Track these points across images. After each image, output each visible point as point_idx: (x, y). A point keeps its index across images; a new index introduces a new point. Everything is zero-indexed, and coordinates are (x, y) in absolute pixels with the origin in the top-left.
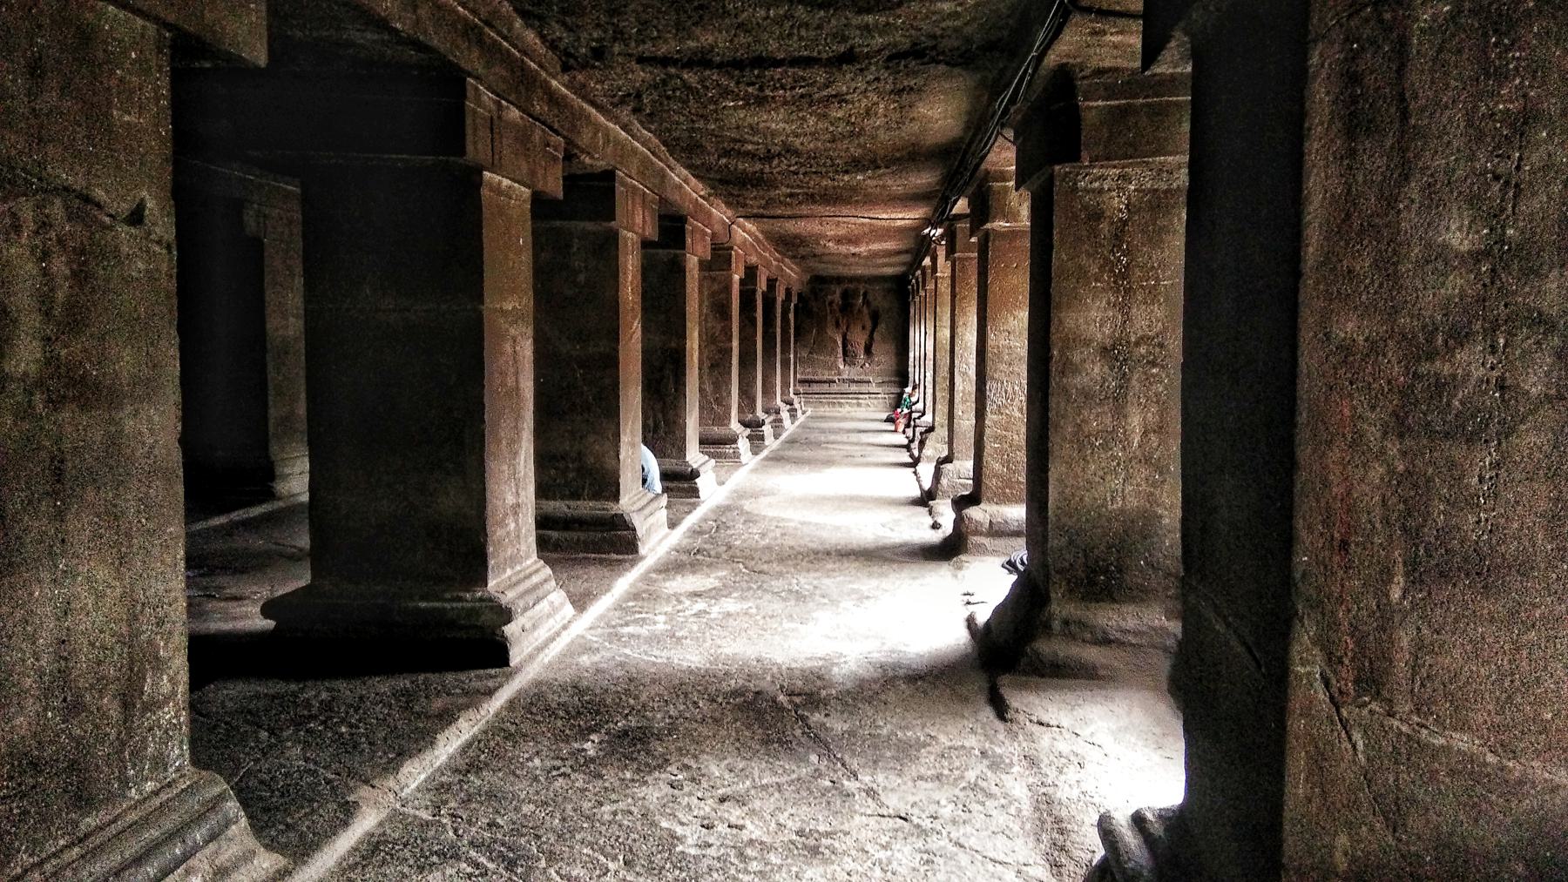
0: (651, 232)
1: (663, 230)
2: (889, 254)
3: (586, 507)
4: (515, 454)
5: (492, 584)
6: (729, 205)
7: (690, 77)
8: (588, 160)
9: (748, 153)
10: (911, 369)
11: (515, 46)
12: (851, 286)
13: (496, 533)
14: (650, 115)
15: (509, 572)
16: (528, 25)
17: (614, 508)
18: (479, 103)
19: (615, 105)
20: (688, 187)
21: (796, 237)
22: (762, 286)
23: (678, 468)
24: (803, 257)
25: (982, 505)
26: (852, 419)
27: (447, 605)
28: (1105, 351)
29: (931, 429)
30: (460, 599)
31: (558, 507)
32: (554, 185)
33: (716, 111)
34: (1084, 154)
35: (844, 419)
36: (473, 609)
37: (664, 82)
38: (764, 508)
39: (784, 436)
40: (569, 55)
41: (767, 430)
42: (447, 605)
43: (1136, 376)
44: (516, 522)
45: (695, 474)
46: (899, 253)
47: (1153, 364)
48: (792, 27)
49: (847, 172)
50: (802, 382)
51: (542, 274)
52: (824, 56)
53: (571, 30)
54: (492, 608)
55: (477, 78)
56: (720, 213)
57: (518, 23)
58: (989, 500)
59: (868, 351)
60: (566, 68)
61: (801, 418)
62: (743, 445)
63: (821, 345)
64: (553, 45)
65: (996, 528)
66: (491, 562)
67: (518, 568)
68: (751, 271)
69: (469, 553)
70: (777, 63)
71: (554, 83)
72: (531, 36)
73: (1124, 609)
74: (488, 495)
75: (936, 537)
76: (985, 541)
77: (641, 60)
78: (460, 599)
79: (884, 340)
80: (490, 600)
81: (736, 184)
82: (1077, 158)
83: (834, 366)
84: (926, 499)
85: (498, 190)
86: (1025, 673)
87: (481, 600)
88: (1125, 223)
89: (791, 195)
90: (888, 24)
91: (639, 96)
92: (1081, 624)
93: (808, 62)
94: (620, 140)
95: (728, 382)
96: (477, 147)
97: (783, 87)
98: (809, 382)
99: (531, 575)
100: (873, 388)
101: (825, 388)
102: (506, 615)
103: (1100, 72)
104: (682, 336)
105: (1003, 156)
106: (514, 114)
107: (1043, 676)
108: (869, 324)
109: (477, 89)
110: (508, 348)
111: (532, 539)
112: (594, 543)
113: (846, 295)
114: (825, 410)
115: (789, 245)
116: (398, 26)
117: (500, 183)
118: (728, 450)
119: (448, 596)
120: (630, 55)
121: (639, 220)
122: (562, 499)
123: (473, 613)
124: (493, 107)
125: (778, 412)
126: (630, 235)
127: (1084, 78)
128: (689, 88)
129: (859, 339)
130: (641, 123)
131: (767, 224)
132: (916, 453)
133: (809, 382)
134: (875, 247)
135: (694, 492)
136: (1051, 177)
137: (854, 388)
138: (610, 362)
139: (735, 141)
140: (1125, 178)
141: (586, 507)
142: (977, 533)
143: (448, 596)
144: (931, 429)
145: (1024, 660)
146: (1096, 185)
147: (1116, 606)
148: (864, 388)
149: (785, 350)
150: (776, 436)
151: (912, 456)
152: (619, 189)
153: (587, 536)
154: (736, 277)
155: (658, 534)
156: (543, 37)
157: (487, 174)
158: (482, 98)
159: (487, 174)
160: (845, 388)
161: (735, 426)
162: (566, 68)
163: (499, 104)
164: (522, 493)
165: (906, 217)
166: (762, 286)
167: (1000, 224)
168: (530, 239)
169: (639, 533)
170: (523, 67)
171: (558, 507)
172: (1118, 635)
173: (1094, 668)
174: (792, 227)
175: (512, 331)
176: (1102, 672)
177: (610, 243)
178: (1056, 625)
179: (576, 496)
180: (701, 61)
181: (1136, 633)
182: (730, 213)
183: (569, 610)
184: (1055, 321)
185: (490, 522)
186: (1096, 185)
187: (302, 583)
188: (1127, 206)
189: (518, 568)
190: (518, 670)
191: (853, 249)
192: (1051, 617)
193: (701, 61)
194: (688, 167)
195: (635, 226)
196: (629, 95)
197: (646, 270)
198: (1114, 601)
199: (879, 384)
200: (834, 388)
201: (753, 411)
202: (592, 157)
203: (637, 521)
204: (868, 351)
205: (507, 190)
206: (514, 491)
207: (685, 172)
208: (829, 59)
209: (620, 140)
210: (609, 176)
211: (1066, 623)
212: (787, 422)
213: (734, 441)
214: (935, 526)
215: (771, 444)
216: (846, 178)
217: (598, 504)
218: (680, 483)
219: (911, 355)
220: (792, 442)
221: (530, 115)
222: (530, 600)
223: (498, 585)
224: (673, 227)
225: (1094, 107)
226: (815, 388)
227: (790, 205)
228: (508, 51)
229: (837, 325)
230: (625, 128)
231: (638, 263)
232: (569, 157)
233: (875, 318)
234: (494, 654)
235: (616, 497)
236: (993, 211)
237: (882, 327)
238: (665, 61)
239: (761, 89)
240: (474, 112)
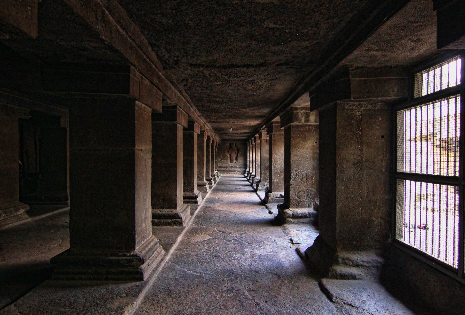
0: (186, 125)
1: (189, 125)
2: (245, 133)
3: (166, 211)
4: (145, 200)
5: (137, 248)
6: (205, 118)
7: (207, 72)
8: (169, 102)
9: (216, 101)
10: (248, 164)
11: (148, 57)
12: (232, 142)
13: (138, 229)
14: (189, 87)
15: (143, 242)
16: (153, 50)
17: (175, 211)
18: (134, 75)
19: (179, 83)
20: (195, 114)
21: (222, 128)
22: (211, 142)
23: (192, 195)
24: (222, 134)
25: (290, 209)
26: (233, 177)
27: (120, 258)
28: (355, 164)
29: (260, 181)
30: (125, 255)
31: (158, 211)
32: (159, 108)
33: (211, 86)
34: (352, 96)
35: (231, 177)
36: (130, 259)
37: (197, 75)
38: (218, 207)
39: (217, 182)
40: (166, 63)
41: (212, 181)
42: (120, 258)
43: (365, 173)
44: (145, 224)
45: (197, 197)
46: (248, 133)
47: (371, 169)
48: (248, 51)
49: (245, 108)
50: (219, 167)
51: (154, 138)
52: (255, 64)
53: (169, 52)
54: (137, 259)
55: (134, 66)
56: (202, 121)
57: (150, 49)
58: (292, 207)
59: (236, 159)
60: (164, 68)
61: (220, 177)
62: (207, 186)
63: (224, 157)
64: (161, 59)
65: (294, 216)
66: (137, 241)
67: (146, 240)
68: (209, 137)
69: (128, 236)
70: (238, 67)
71: (160, 74)
72: (153, 54)
73: (362, 253)
74: (136, 217)
75: (259, 200)
76: (291, 220)
77: (191, 65)
78: (125, 255)
79: (241, 156)
80: (136, 255)
81: (208, 113)
82: (349, 97)
83: (227, 163)
84: (264, 203)
85: (140, 108)
86: (331, 278)
87: (133, 256)
88: (361, 120)
89: (225, 116)
90: (282, 50)
91: (187, 80)
92: (348, 259)
93: (249, 66)
94: (177, 96)
95: (203, 169)
96: (134, 91)
97: (237, 77)
98: (221, 167)
99: (150, 243)
100: (238, 169)
101: (225, 169)
102: (142, 261)
103: (357, 68)
104: (193, 156)
105: (304, 102)
106: (147, 82)
107: (337, 279)
108: (237, 152)
109: (134, 71)
110: (143, 162)
111: (150, 222)
112: (169, 223)
113: (230, 144)
114: (225, 175)
115: (218, 130)
116: (103, 38)
117: (142, 105)
118: (203, 188)
119: (120, 254)
120: (188, 63)
121: (183, 121)
122: (158, 209)
123: (130, 261)
124: (140, 78)
125: (214, 176)
126: (180, 126)
127: (352, 70)
128: (205, 77)
129: (234, 156)
130: (185, 90)
131: (214, 124)
132: (255, 187)
133: (221, 167)
134: (243, 131)
135: (196, 202)
136: (336, 105)
137: (233, 169)
138: (175, 165)
139: (214, 97)
140: (360, 106)
141: (166, 211)
142: (289, 217)
143: (120, 254)
144: (260, 181)
145: (330, 273)
146: (351, 108)
147: (359, 252)
148: (236, 169)
149: (216, 159)
150: (215, 183)
151: (253, 188)
152: (178, 111)
153: (166, 219)
154: (205, 139)
155: (188, 221)
156: (157, 55)
157: (137, 102)
158: (135, 75)
159: (137, 102)
160: (231, 169)
161: (205, 181)
162: (164, 68)
163: (142, 78)
164: (148, 213)
165: (254, 123)
166: (211, 142)
167: (295, 123)
168: (151, 126)
169: (183, 219)
170: (151, 67)
171: (158, 211)
172: (362, 263)
173: (355, 276)
174: (222, 125)
175: (145, 157)
176: (357, 277)
177: (175, 128)
178: (340, 260)
179: (162, 208)
180: (211, 65)
181: (368, 262)
182: (205, 121)
183: (163, 252)
184: (338, 154)
185: (136, 226)
186: (351, 108)
187: (65, 249)
188: (361, 115)
189: (146, 240)
190: (147, 282)
191: (236, 132)
192: (338, 257)
193: (211, 65)
194: (196, 106)
195: (182, 123)
196: (184, 80)
197: (184, 135)
198: (358, 250)
199: (239, 168)
200: (228, 169)
201: (209, 176)
202: (170, 100)
203: (182, 215)
204: (236, 159)
205: (144, 110)
206: (144, 210)
207: (195, 108)
208: (256, 65)
209: (177, 96)
210: (175, 107)
211: (343, 259)
212: (217, 179)
213: (205, 185)
214: (270, 213)
215: (214, 185)
216: (244, 110)
217: (169, 210)
218: (191, 200)
219: (248, 160)
220: (218, 184)
221: (153, 83)
222: (150, 253)
223: (139, 249)
224: (191, 123)
225: (355, 80)
226: (223, 169)
227: (224, 119)
228: (145, 59)
229: (228, 152)
230: (180, 92)
231: (182, 135)
232: (163, 100)
233: (238, 150)
234: (138, 276)
235: (175, 208)
236: (293, 119)
237: (240, 153)
238: (199, 66)
239: (229, 77)
240: (133, 79)
